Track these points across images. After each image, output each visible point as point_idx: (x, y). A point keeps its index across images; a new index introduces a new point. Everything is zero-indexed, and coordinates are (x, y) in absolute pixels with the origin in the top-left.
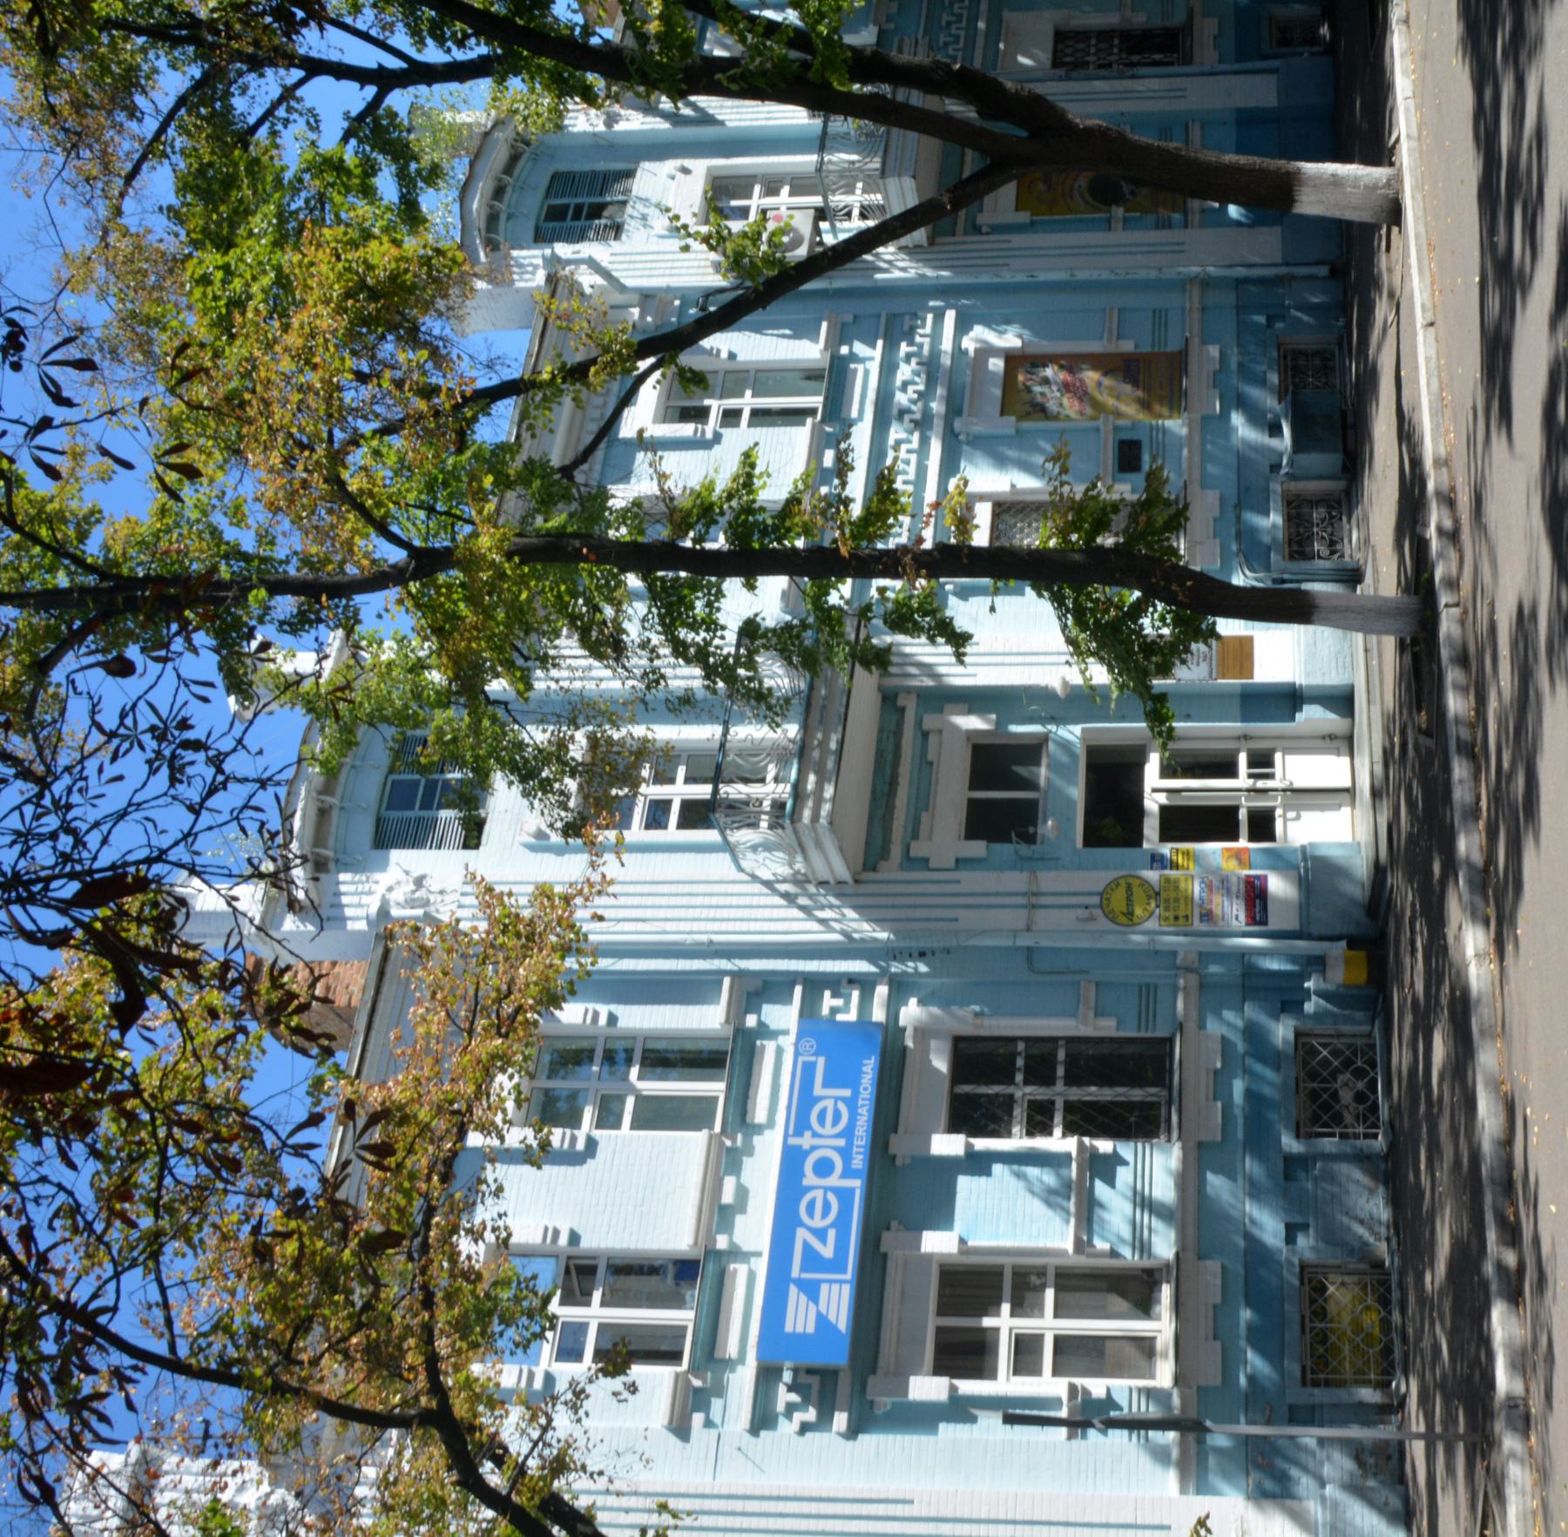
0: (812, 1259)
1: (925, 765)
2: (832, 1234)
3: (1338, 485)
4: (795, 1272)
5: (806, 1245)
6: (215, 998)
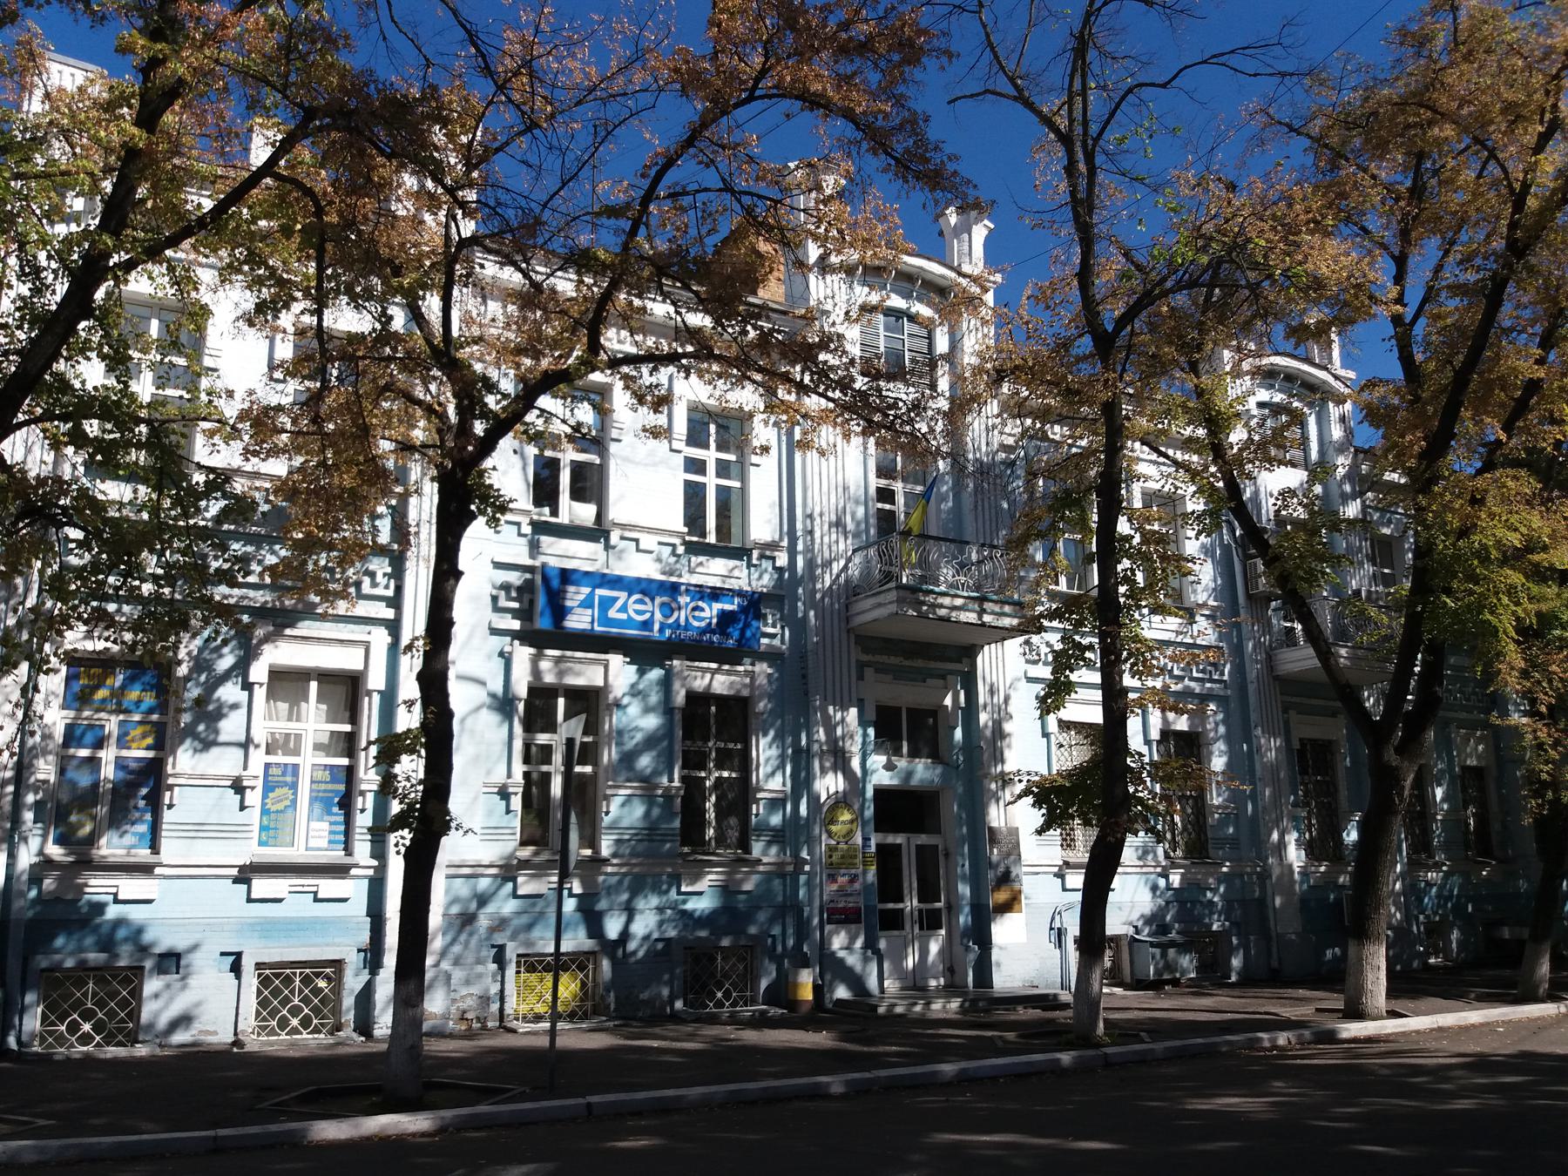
0: (606, 603)
1: (923, 676)
2: (623, 616)
3: (1128, 979)
4: (600, 592)
5: (616, 599)
6: (693, 232)
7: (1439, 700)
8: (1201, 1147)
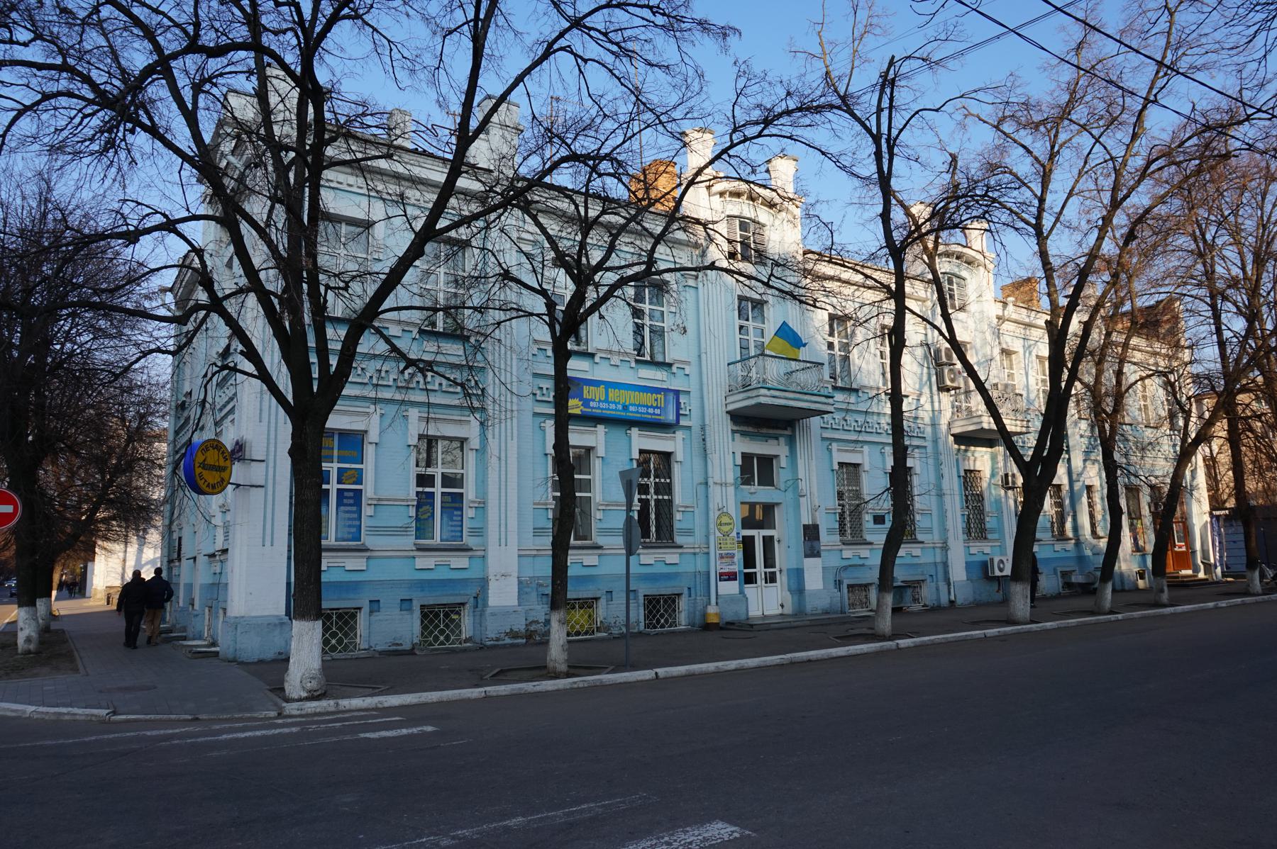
7: (906, 448)
8: (368, 735)
